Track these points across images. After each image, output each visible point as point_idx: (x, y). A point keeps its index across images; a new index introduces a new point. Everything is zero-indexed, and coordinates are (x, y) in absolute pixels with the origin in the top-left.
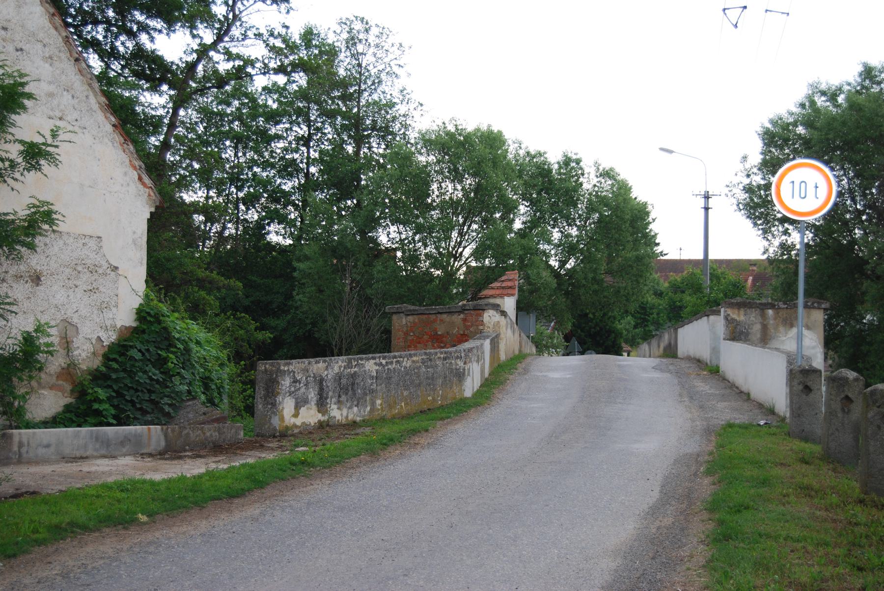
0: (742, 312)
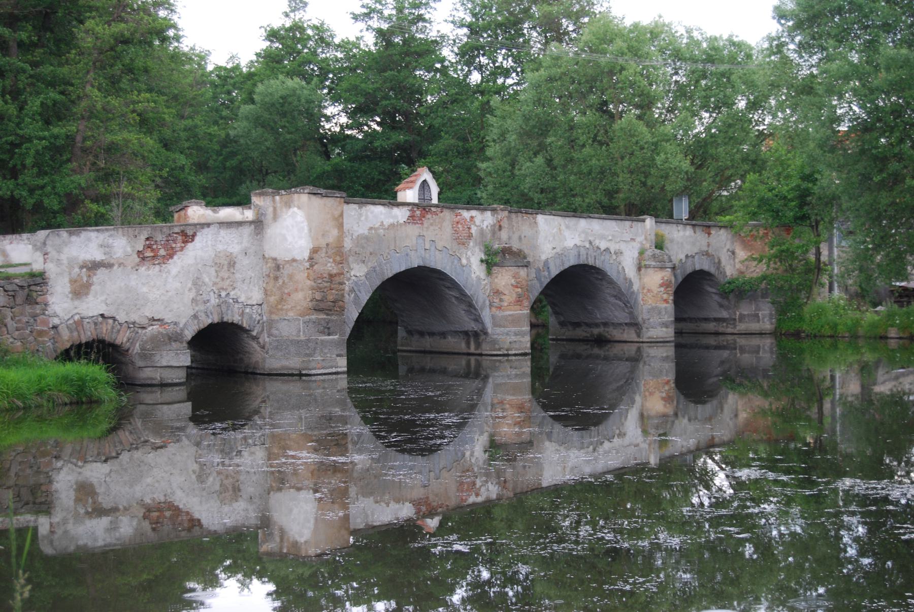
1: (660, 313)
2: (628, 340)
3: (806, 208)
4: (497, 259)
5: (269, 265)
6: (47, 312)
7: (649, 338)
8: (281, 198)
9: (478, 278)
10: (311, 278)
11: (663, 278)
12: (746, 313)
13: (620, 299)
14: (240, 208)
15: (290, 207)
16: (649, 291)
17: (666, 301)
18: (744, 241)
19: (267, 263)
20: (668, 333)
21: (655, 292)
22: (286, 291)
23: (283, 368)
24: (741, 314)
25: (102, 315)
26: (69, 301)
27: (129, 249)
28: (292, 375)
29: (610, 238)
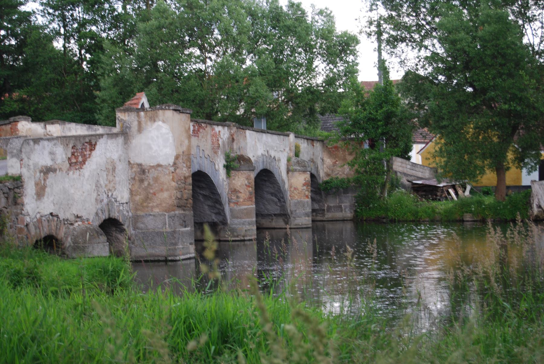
0: (127, 114)
1: (304, 206)
2: (276, 227)
3: (389, 126)
4: (235, 164)
5: (134, 169)
6: (23, 212)
7: (296, 225)
8: (146, 114)
9: (223, 179)
10: (175, 180)
11: (305, 180)
12: (332, 205)
13: (276, 196)
14: (42, 124)
15: (155, 121)
16: (295, 189)
17: (307, 196)
18: (330, 151)
19: (132, 168)
20: (307, 221)
21: (300, 190)
22: (151, 191)
23: (151, 255)
24: (328, 206)
25: (51, 214)
26: (34, 201)
27: (64, 156)
28: (159, 261)
29: (276, 149)
